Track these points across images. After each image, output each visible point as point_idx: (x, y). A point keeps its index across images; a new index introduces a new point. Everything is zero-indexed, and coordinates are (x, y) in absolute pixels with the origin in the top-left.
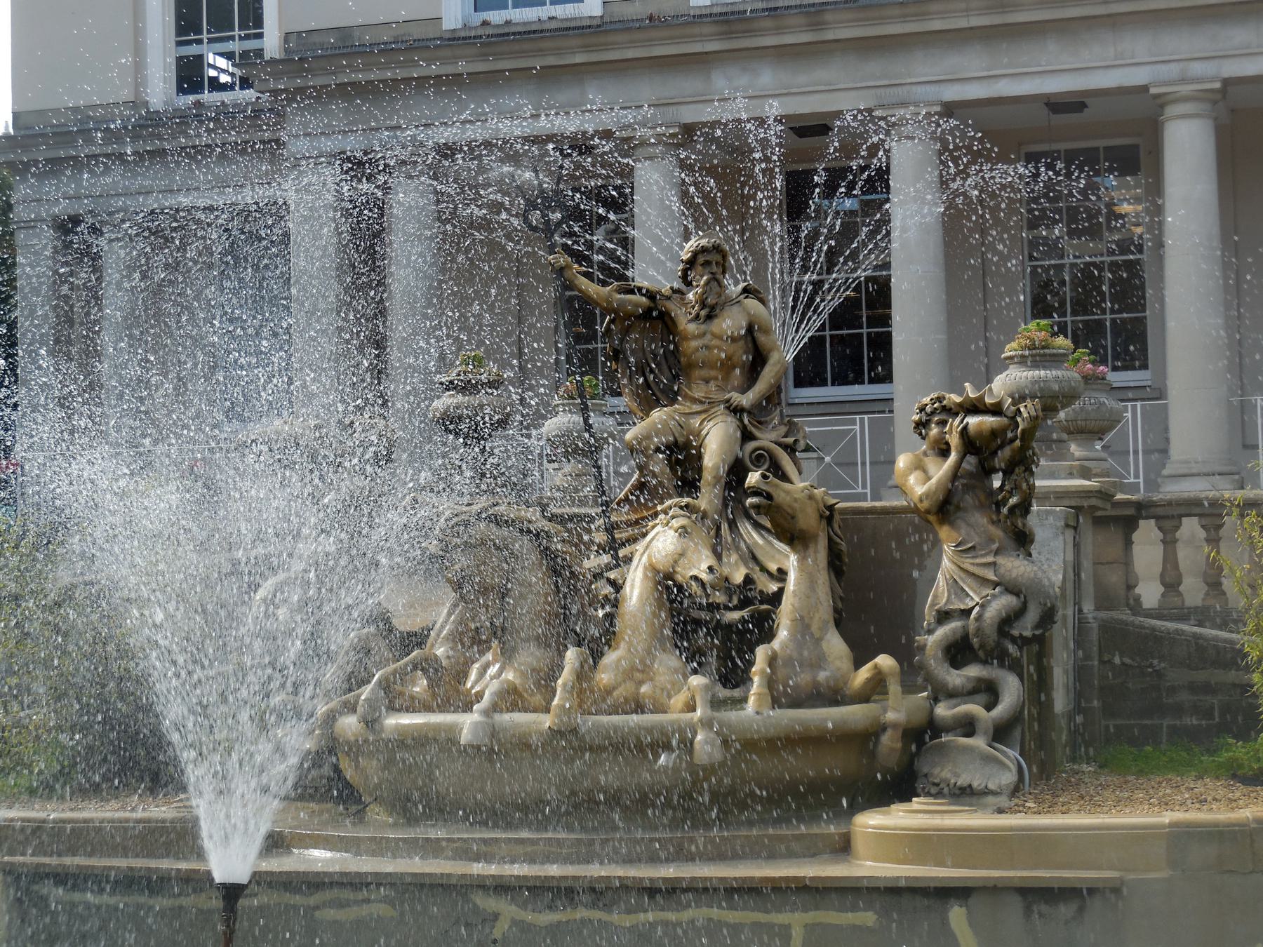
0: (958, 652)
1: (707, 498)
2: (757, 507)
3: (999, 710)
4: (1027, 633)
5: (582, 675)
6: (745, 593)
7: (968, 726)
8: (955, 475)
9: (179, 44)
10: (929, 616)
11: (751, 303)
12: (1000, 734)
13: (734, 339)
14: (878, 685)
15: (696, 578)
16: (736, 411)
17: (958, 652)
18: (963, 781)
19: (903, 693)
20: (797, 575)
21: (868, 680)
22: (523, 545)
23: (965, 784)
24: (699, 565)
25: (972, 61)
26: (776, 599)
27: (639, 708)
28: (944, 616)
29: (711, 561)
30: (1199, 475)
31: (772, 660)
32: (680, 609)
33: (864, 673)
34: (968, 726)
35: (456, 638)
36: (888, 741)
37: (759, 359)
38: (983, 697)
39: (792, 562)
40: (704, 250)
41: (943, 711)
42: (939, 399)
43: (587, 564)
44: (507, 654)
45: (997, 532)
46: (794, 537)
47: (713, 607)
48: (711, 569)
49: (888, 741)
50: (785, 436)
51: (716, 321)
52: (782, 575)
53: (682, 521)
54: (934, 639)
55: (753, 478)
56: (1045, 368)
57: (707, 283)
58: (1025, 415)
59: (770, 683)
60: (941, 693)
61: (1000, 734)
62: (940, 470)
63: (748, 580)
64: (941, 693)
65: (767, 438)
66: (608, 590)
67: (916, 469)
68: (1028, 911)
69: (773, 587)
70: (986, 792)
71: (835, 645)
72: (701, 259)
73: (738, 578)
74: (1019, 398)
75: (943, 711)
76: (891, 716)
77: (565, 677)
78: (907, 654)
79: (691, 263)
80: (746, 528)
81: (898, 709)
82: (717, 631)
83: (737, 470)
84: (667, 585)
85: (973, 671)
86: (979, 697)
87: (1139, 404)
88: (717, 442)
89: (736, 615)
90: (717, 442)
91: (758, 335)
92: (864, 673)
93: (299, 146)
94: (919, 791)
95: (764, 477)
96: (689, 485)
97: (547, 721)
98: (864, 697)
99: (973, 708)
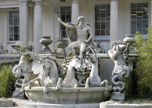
1: (81, 56)
2: (88, 57)
3: (122, 88)
4: (127, 77)
5: (61, 82)
6: (86, 70)
7: (117, 90)
8: (117, 53)
10: (113, 74)
11: (88, 27)
12: (122, 92)
13: (85, 32)
14: (104, 85)
15: (78, 68)
16: (85, 43)
17: (117, 80)
18: (116, 99)
20: (93, 69)
21: (103, 83)
22: (54, 63)
23: (117, 99)
26: (90, 71)
27: (69, 87)
28: (114, 74)
29: (80, 65)
31: (89, 80)
32: (76, 73)
33: (103, 82)
34: (117, 90)
35: (43, 75)
36: (106, 92)
37: (89, 35)
38: (121, 86)
39: (93, 66)
40: (81, 18)
41: (115, 88)
42: (115, 42)
43: (62, 65)
44: (50, 78)
46: (94, 62)
48: (80, 66)
49: (106, 92)
50: (93, 47)
51: (83, 29)
52: (91, 67)
53: (76, 59)
54: (113, 78)
55: (87, 53)
56: (131, 37)
57: (81, 23)
58: (128, 45)
61: (122, 92)
62: (115, 52)
63: (86, 68)
64: (114, 85)
65: (90, 47)
66: (65, 69)
67: (111, 52)
69: (90, 69)
70: (120, 100)
71: (99, 78)
72: (81, 20)
73: (85, 68)
74: (127, 42)
75: (115, 88)
77: (59, 82)
78: (109, 80)
79: (79, 21)
80: (86, 60)
82: (80, 75)
83: (84, 53)
85: (118, 82)
86: (119, 86)
87: (66, 58)
88: (82, 47)
89: (84, 73)
90: (82, 47)
91: (89, 31)
92: (103, 82)
94: (79, 52)
95: (89, 53)
96: (78, 54)
97: (56, 88)
98: (102, 86)
99: (118, 88)
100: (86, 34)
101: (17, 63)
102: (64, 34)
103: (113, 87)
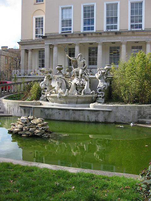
0: (100, 91)
1: (79, 77)
7: (100, 97)
9: (36, 34)
12: (103, 98)
14: (93, 94)
16: (82, 69)
17: (100, 91)
19: (8, 133)
20: (87, 84)
24: (78, 82)
25: (105, 38)
26: (85, 85)
28: (99, 87)
30: (59, 120)
33: (92, 92)
34: (100, 97)
36: (93, 98)
37: (84, 65)
41: (99, 96)
45: (104, 80)
47: (79, 86)
49: (93, 98)
55: (83, 75)
59: (84, 93)
60: (98, 94)
61: (103, 98)
64: (98, 94)
65: (85, 71)
68: (69, 10)
71: (89, 90)
74: (106, 69)
76: (94, 96)
78: (96, 91)
81: (94, 95)
84: (75, 84)
85: (101, 92)
88: (80, 71)
92: (92, 92)
93: (45, 44)
96: (78, 75)
97: (65, 95)
98: (91, 94)
100: (83, 64)
101: (43, 80)
102: (70, 64)
103: (98, 95)
